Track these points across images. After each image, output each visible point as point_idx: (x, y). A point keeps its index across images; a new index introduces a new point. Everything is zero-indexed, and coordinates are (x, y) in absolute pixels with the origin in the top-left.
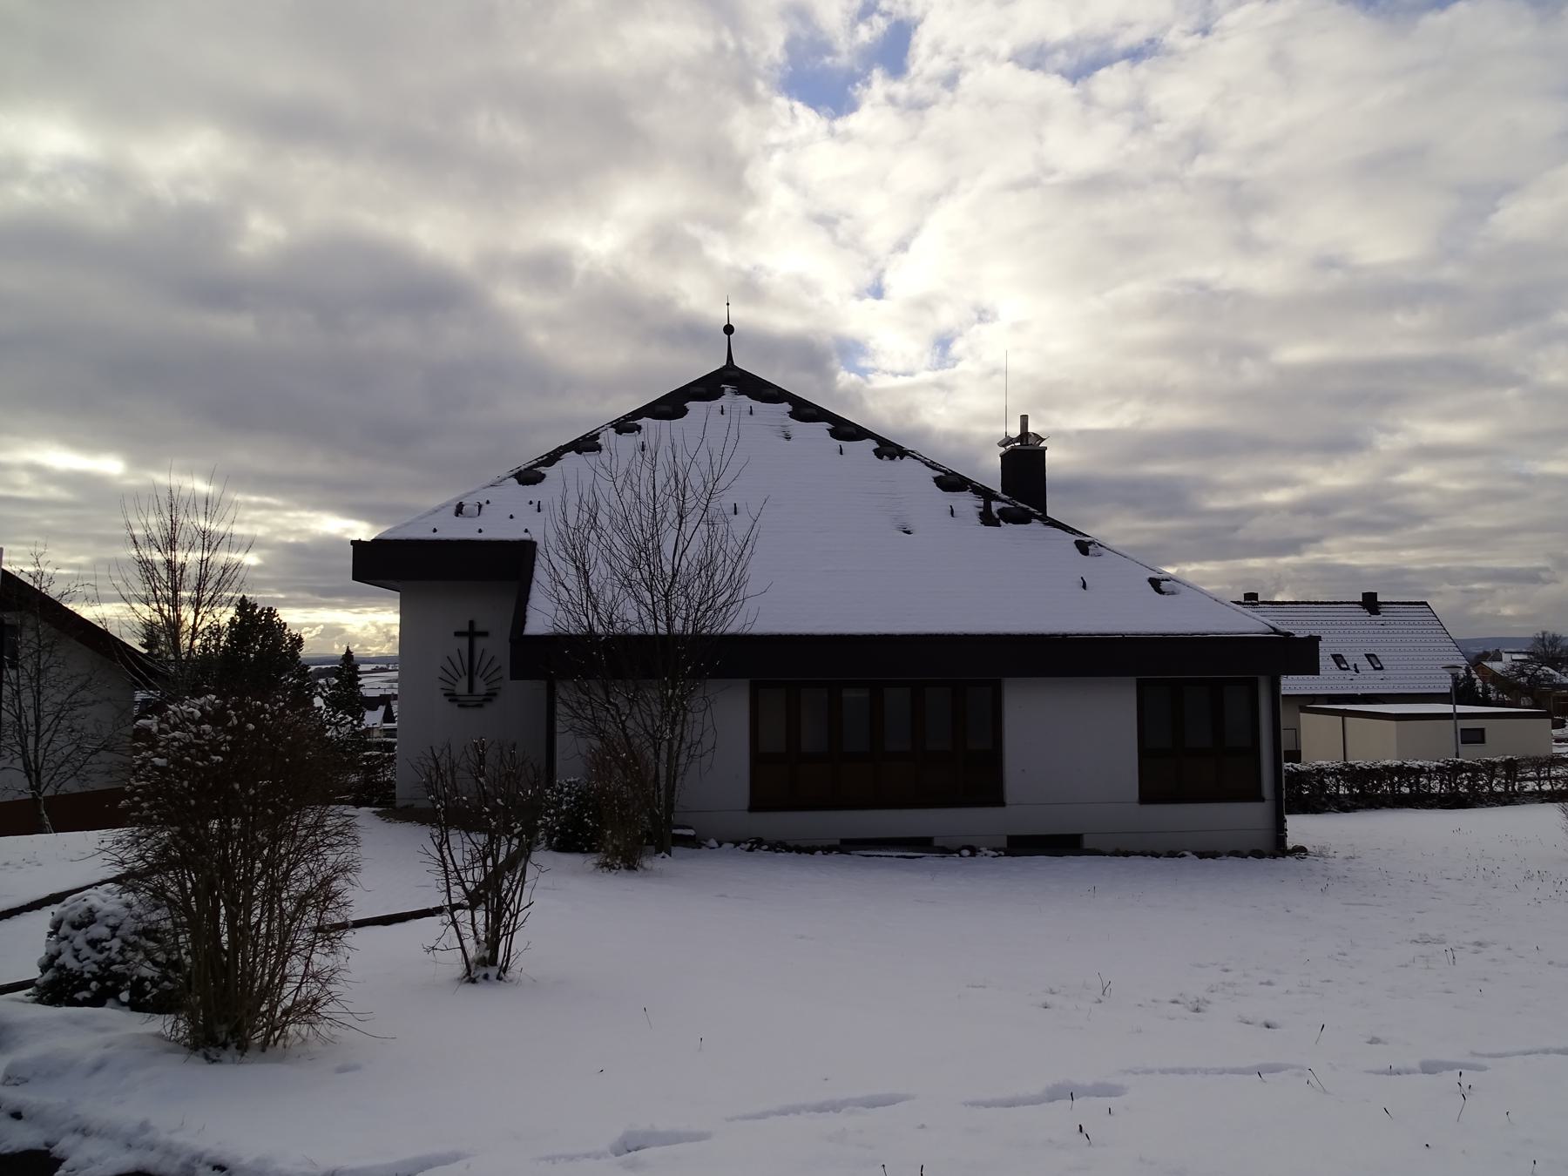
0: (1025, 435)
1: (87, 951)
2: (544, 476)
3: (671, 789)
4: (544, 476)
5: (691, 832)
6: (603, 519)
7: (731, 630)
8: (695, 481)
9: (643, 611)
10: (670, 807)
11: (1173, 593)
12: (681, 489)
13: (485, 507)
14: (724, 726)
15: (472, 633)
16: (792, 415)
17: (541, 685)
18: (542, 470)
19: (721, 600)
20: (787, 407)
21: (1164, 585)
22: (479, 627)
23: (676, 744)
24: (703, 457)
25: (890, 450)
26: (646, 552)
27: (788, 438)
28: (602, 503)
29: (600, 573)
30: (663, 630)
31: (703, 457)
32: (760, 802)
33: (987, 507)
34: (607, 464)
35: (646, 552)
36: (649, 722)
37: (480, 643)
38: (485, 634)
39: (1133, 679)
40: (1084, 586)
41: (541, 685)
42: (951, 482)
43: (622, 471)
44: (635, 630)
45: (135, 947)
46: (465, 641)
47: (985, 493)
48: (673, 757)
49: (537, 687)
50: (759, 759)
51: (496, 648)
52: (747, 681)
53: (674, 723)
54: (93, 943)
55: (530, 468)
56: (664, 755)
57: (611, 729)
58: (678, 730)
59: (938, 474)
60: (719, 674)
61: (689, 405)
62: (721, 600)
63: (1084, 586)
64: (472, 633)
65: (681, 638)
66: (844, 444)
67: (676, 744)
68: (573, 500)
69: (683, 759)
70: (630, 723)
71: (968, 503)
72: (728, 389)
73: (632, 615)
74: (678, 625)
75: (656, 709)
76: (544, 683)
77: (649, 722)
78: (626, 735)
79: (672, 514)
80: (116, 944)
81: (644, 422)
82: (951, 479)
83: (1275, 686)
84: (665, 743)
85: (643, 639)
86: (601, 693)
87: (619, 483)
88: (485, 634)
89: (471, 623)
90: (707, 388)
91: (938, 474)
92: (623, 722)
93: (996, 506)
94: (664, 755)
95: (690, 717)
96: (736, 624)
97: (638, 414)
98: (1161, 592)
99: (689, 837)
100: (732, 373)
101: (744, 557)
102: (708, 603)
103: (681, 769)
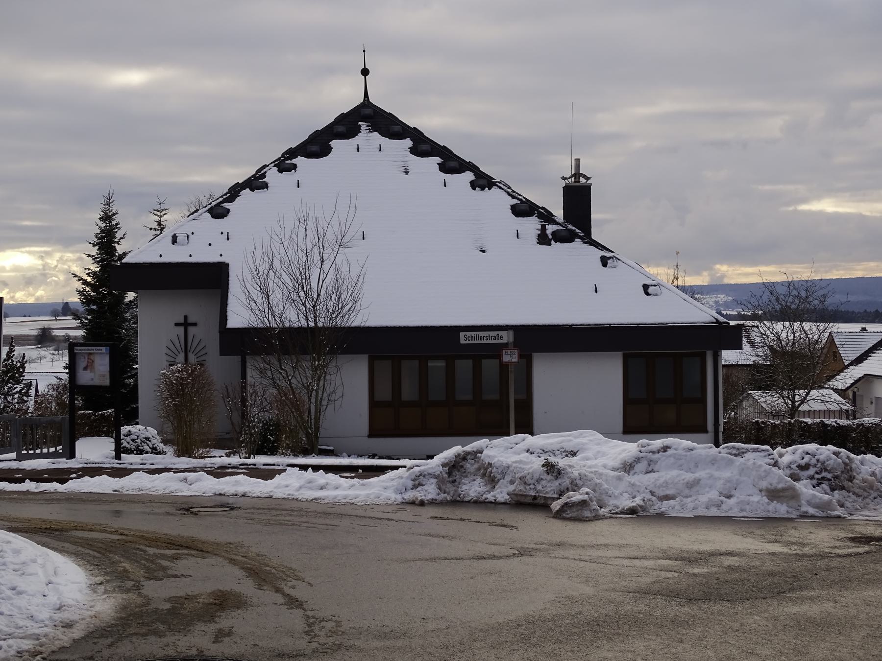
0: (577, 175)
1: (131, 442)
2: (228, 211)
3: (317, 420)
4: (228, 211)
5: (331, 448)
6: (277, 264)
7: (353, 325)
8: (330, 236)
9: (301, 316)
10: (317, 429)
11: (656, 295)
12: (321, 239)
13: (191, 237)
14: (350, 386)
15: (186, 324)
16: (414, 151)
17: (237, 359)
18: (227, 205)
19: (348, 307)
20: (408, 143)
21: (651, 290)
22: (190, 320)
23: (320, 393)
24: (335, 222)
25: (482, 182)
26: (301, 283)
27: (406, 172)
28: (277, 255)
29: (276, 297)
30: (312, 324)
31: (335, 222)
32: (373, 433)
33: (543, 229)
34: (279, 234)
35: (301, 283)
36: (305, 381)
37: (191, 330)
38: (195, 324)
39: (621, 353)
40: (596, 291)
41: (237, 359)
42: (524, 209)
43: (287, 237)
44: (295, 326)
45: (144, 442)
46: (181, 329)
47: (547, 217)
48: (318, 404)
49: (234, 361)
50: (374, 405)
51: (206, 335)
52: (366, 356)
53: (319, 380)
54: (133, 440)
55: (218, 205)
56: (313, 400)
57: (283, 384)
58: (321, 383)
59: (516, 201)
60: (346, 352)
61: (334, 143)
62: (348, 307)
63: (596, 291)
64: (186, 324)
65: (324, 328)
66: (448, 177)
67: (320, 393)
68: (259, 254)
69: (324, 403)
70: (294, 381)
71: (532, 224)
72: (363, 126)
73: (294, 318)
74: (320, 324)
75: (309, 373)
76: (457, 361)
77: (305, 381)
78: (292, 387)
79: (317, 258)
80: (139, 441)
81: (299, 161)
82: (524, 207)
83: (716, 357)
84: (314, 393)
85: (300, 329)
86: (276, 363)
87: (286, 244)
88: (195, 324)
89: (186, 317)
90: (346, 126)
91: (516, 201)
92: (290, 380)
93: (550, 228)
94: (313, 400)
95: (328, 377)
96: (357, 321)
97: (292, 153)
98: (647, 294)
99: (330, 450)
100: (368, 111)
101: (359, 284)
102: (339, 309)
103: (324, 408)
